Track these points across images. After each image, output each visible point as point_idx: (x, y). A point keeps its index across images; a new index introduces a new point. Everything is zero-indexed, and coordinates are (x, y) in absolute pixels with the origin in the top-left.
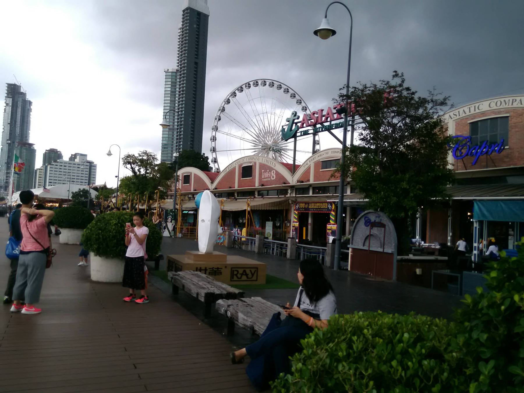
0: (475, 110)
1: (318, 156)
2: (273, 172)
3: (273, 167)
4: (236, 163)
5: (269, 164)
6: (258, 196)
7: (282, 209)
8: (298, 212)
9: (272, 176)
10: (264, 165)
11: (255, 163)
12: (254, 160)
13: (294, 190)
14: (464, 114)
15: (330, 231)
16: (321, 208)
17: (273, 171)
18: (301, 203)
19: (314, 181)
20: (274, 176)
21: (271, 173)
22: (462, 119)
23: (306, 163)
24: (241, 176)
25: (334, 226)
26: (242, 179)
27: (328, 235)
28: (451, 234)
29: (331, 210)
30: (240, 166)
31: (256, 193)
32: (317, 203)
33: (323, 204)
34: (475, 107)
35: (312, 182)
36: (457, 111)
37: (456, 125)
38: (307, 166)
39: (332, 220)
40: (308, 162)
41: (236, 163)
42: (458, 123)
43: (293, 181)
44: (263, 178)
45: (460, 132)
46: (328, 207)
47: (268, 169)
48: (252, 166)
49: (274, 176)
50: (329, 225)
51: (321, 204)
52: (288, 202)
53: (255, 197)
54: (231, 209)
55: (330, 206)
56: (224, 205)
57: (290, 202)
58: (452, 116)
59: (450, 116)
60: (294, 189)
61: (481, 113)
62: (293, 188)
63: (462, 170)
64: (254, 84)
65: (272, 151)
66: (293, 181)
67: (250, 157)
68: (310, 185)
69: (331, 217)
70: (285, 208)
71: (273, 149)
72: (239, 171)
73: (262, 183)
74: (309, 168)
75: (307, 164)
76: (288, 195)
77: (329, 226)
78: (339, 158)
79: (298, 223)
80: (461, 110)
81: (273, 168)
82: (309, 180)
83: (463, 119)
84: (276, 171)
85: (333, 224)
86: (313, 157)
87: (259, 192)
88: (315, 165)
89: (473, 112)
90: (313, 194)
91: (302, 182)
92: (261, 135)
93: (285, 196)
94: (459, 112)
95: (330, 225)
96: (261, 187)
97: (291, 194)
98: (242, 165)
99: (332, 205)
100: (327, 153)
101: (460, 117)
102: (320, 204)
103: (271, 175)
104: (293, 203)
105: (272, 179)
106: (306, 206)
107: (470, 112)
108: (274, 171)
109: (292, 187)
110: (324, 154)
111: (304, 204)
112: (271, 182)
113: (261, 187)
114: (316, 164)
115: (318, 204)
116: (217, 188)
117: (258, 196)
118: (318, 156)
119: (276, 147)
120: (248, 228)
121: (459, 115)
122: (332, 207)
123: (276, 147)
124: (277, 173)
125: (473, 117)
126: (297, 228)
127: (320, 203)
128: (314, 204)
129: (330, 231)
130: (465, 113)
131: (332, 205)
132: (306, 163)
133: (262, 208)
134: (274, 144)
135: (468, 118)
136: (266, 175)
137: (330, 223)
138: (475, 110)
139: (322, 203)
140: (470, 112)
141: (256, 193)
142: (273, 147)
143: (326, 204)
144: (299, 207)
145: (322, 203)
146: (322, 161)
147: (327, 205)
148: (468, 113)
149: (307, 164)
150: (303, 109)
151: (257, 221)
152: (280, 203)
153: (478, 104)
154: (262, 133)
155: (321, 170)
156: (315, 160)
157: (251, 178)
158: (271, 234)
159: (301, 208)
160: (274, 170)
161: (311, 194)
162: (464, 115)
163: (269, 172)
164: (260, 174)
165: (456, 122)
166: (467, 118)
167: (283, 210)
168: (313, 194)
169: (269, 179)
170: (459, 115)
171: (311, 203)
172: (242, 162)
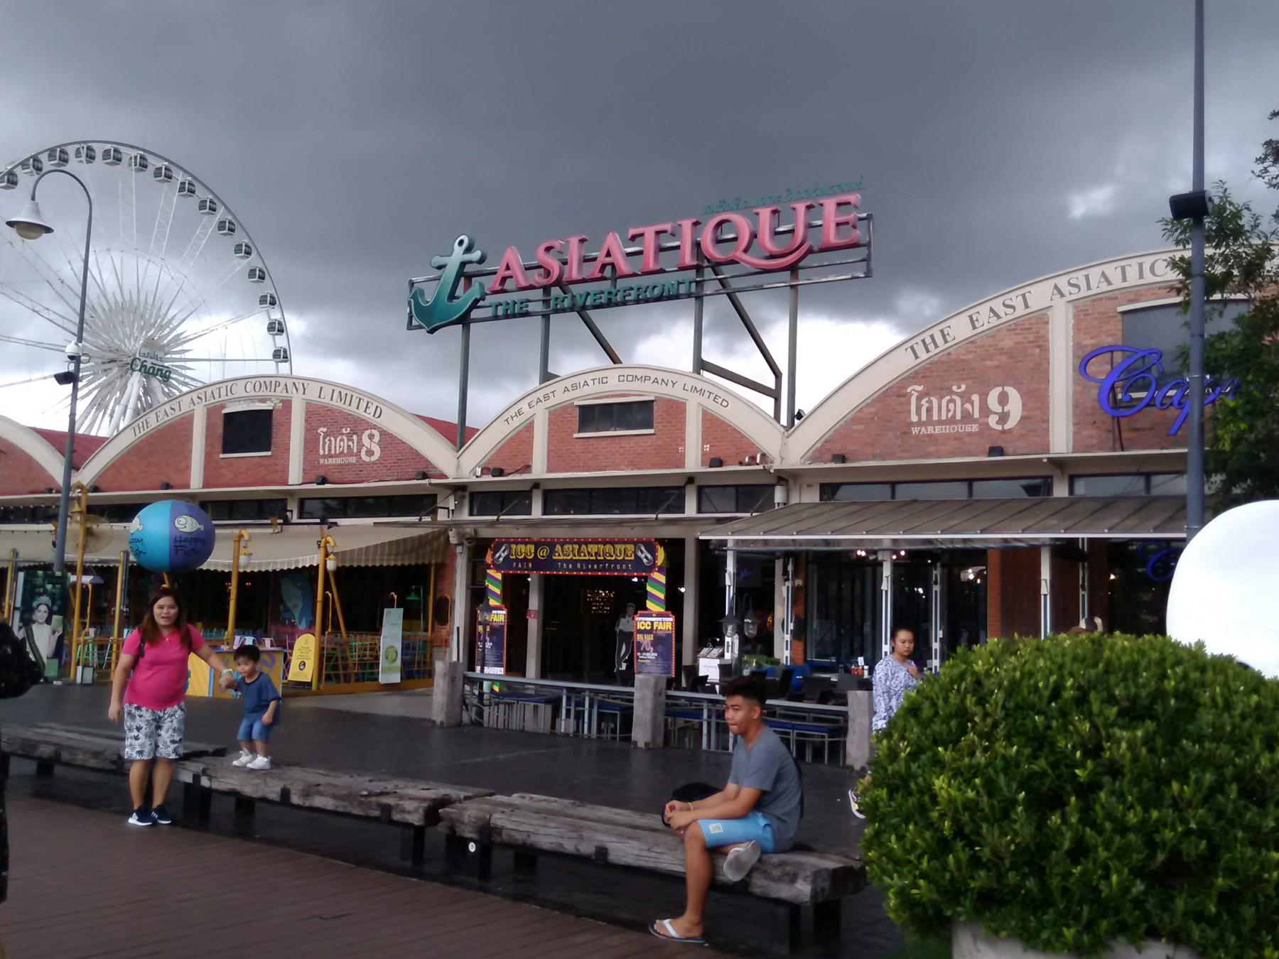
0: (1141, 277)
1: (566, 389)
2: (371, 437)
3: (369, 416)
4: (196, 400)
5: (353, 408)
6: (300, 517)
7: (427, 562)
8: (504, 575)
9: (364, 450)
10: (330, 410)
11: (287, 404)
12: (280, 392)
13: (464, 497)
14: (1106, 284)
15: (650, 638)
16: (605, 561)
17: (367, 432)
18: (517, 543)
19: (549, 470)
20: (371, 448)
21: (360, 440)
22: (1098, 299)
23: (515, 409)
24: (219, 444)
25: (499, 612)
26: (222, 456)
27: (639, 650)
28: (940, 634)
29: (651, 568)
30: (211, 412)
31: (293, 506)
32: (587, 543)
33: (618, 547)
34: (1141, 265)
35: (539, 470)
36: (1081, 275)
37: (1076, 316)
38: (517, 422)
39: (656, 599)
40: (524, 405)
41: (196, 400)
42: (1083, 310)
43: (458, 467)
44: (324, 456)
45: (1092, 338)
46: (636, 556)
47: (346, 425)
48: (270, 412)
49: (371, 448)
50: (642, 616)
51: (608, 547)
52: (442, 539)
53: (287, 522)
54: (106, 561)
55: (644, 555)
56: (249, 550)
57: (453, 540)
58: (1066, 289)
59: (1056, 287)
60: (467, 494)
61: (1158, 285)
62: (460, 493)
63: (1101, 449)
64: (106, 153)
65: (140, 370)
66: (458, 467)
67: (262, 380)
68: (536, 484)
69: (649, 589)
70: (433, 562)
71: (142, 366)
72: (209, 427)
73: (322, 472)
74: (529, 427)
75: (519, 413)
76: (442, 516)
77: (644, 619)
78: (653, 398)
79: (504, 612)
80: (1095, 274)
81: (368, 423)
82: (527, 468)
83: (1102, 299)
84: (383, 433)
85: (659, 615)
86: (540, 394)
87: (302, 502)
88: (550, 422)
89: (1133, 279)
90: (545, 513)
91: (501, 472)
92: (97, 325)
93: (434, 519)
94: (1087, 277)
95: (650, 616)
96: (315, 486)
97: (450, 512)
98: (223, 407)
99: (653, 551)
100: (601, 381)
101: (1091, 293)
102: (601, 547)
103: (360, 445)
104: (461, 544)
105: (365, 458)
106: (543, 554)
107: (1124, 279)
108: (376, 433)
109: (458, 489)
110: (591, 383)
111: (532, 547)
112: (362, 470)
113: (315, 486)
114: (556, 416)
115: (593, 548)
116: (102, 486)
117: (300, 517)
118: (566, 389)
119: (154, 361)
120: (323, 633)
121: (1089, 288)
122: (655, 558)
123: (154, 361)
124: (388, 440)
125: (1132, 297)
126: (502, 627)
127: (604, 542)
128: (577, 547)
129: (650, 638)
130: (1109, 283)
131: (653, 551)
132: (515, 409)
133: (374, 560)
134: (145, 351)
135: (1116, 298)
136: (340, 444)
137: (646, 609)
138: (1141, 277)
139: (612, 542)
140: (1124, 279)
141: (293, 506)
142: (143, 359)
143: (631, 547)
144: (506, 558)
145: (612, 542)
146: (581, 407)
147: (635, 552)
148: (1117, 283)
149: (519, 413)
150: (240, 251)
151: (300, 604)
152: (422, 541)
153: (1152, 259)
154: (99, 317)
155: (576, 435)
156: (553, 401)
157: (269, 453)
158: (396, 652)
159: (517, 560)
160: (375, 427)
161: (537, 512)
162: (1104, 287)
163: (350, 437)
164: (311, 444)
165: (1076, 307)
166: (1112, 297)
167: (430, 564)
168: (545, 513)
169: (353, 460)
170: (1089, 288)
171: (562, 544)
172: (223, 397)
